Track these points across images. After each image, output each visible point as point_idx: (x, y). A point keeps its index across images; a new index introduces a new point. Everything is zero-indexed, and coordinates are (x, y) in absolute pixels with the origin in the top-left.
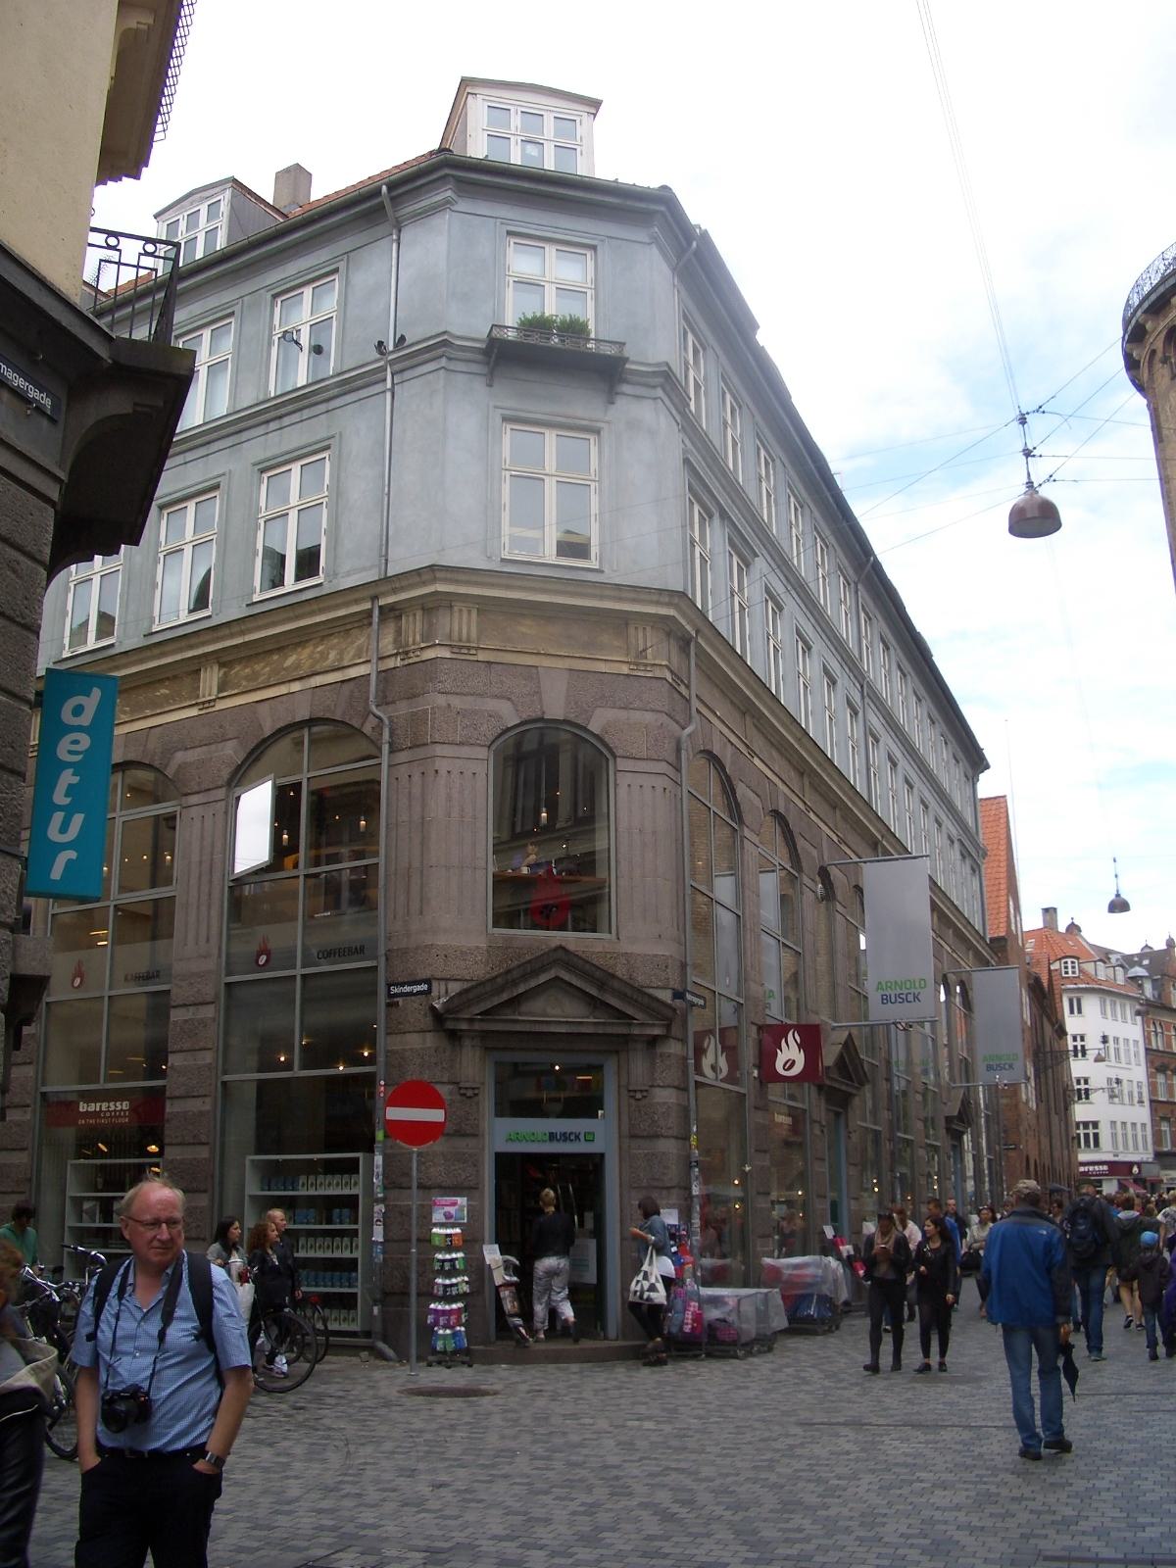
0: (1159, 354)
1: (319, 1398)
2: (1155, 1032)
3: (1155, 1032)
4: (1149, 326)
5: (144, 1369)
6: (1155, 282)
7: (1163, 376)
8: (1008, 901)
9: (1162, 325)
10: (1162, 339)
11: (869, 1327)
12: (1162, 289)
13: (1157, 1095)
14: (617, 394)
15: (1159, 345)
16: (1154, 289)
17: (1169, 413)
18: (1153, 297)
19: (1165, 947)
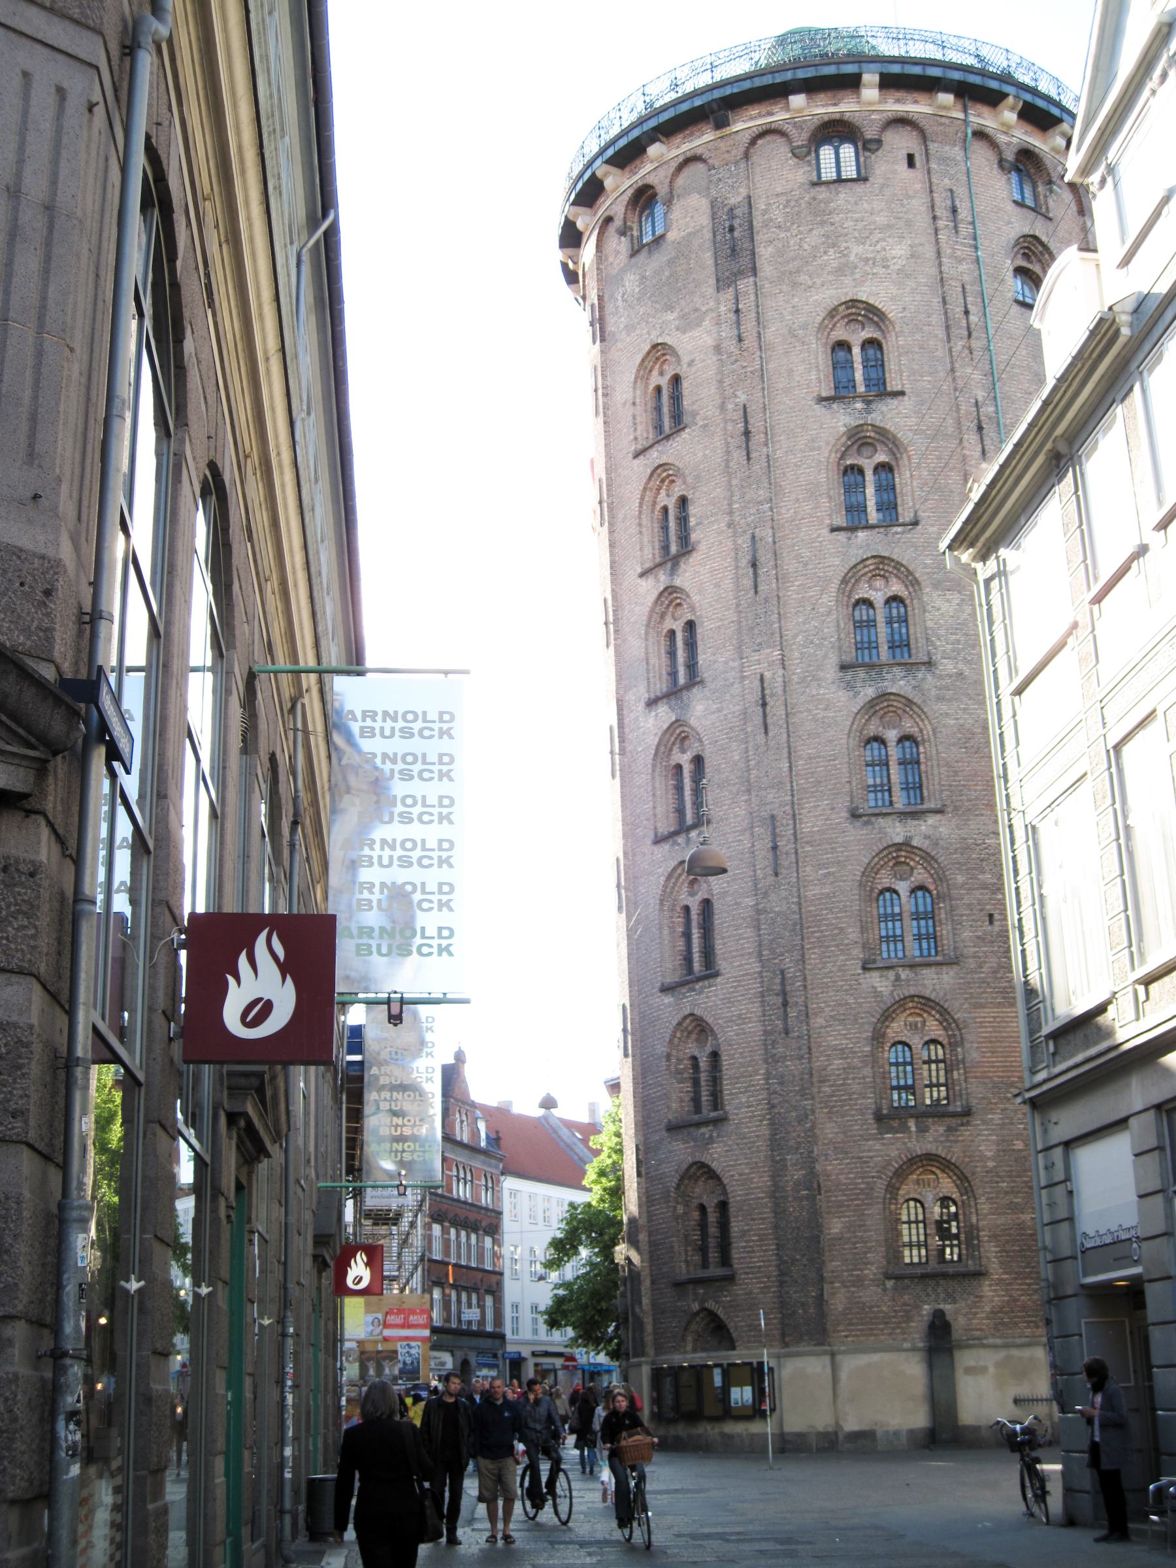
0: (618, 222)
1: (765, 212)
2: (457, 1177)
3: (457, 1177)
4: (608, 183)
5: (44, 1180)
6: (626, 124)
7: (618, 253)
8: (416, 1268)
9: (628, 183)
10: (625, 203)
11: (184, 310)
12: (636, 133)
13: (483, 1263)
14: (1160, 1148)
15: (619, 210)
16: (624, 133)
17: (620, 303)
18: (622, 143)
19: (453, 1061)
